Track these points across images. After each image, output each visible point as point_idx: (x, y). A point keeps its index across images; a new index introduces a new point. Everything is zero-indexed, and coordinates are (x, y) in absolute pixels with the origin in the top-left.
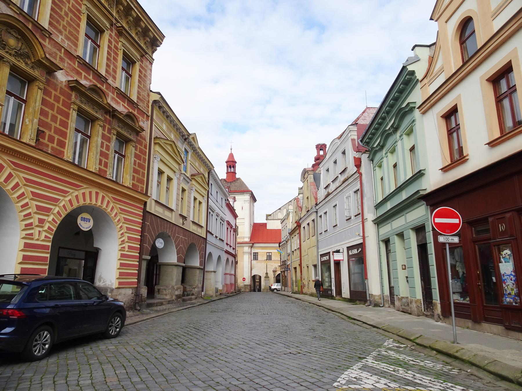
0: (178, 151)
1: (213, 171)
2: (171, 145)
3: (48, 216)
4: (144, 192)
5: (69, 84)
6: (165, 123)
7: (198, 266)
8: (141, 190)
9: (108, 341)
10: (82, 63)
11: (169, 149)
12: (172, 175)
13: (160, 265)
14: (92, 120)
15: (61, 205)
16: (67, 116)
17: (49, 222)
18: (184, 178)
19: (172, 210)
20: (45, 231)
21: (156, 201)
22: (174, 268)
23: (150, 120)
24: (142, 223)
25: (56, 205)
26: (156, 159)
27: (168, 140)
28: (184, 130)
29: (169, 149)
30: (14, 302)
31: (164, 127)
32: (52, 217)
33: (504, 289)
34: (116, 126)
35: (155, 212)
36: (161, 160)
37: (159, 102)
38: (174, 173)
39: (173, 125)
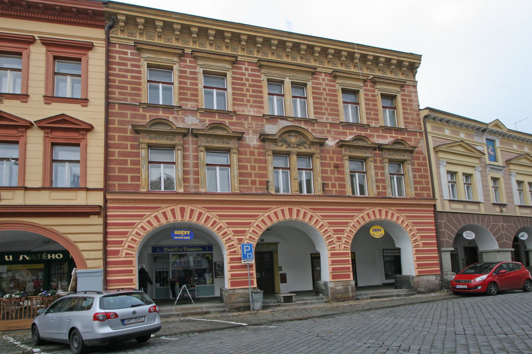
0: (467, 144)
2: (460, 145)
3: (343, 234)
4: (432, 196)
5: (338, 144)
6: (462, 132)
10: (146, 107)
12: (468, 171)
15: (351, 225)
16: (138, 155)
17: (345, 238)
18: (491, 168)
20: (344, 244)
21: (450, 201)
24: (435, 222)
25: (347, 226)
31: (515, 147)
32: (346, 234)
34: (387, 155)
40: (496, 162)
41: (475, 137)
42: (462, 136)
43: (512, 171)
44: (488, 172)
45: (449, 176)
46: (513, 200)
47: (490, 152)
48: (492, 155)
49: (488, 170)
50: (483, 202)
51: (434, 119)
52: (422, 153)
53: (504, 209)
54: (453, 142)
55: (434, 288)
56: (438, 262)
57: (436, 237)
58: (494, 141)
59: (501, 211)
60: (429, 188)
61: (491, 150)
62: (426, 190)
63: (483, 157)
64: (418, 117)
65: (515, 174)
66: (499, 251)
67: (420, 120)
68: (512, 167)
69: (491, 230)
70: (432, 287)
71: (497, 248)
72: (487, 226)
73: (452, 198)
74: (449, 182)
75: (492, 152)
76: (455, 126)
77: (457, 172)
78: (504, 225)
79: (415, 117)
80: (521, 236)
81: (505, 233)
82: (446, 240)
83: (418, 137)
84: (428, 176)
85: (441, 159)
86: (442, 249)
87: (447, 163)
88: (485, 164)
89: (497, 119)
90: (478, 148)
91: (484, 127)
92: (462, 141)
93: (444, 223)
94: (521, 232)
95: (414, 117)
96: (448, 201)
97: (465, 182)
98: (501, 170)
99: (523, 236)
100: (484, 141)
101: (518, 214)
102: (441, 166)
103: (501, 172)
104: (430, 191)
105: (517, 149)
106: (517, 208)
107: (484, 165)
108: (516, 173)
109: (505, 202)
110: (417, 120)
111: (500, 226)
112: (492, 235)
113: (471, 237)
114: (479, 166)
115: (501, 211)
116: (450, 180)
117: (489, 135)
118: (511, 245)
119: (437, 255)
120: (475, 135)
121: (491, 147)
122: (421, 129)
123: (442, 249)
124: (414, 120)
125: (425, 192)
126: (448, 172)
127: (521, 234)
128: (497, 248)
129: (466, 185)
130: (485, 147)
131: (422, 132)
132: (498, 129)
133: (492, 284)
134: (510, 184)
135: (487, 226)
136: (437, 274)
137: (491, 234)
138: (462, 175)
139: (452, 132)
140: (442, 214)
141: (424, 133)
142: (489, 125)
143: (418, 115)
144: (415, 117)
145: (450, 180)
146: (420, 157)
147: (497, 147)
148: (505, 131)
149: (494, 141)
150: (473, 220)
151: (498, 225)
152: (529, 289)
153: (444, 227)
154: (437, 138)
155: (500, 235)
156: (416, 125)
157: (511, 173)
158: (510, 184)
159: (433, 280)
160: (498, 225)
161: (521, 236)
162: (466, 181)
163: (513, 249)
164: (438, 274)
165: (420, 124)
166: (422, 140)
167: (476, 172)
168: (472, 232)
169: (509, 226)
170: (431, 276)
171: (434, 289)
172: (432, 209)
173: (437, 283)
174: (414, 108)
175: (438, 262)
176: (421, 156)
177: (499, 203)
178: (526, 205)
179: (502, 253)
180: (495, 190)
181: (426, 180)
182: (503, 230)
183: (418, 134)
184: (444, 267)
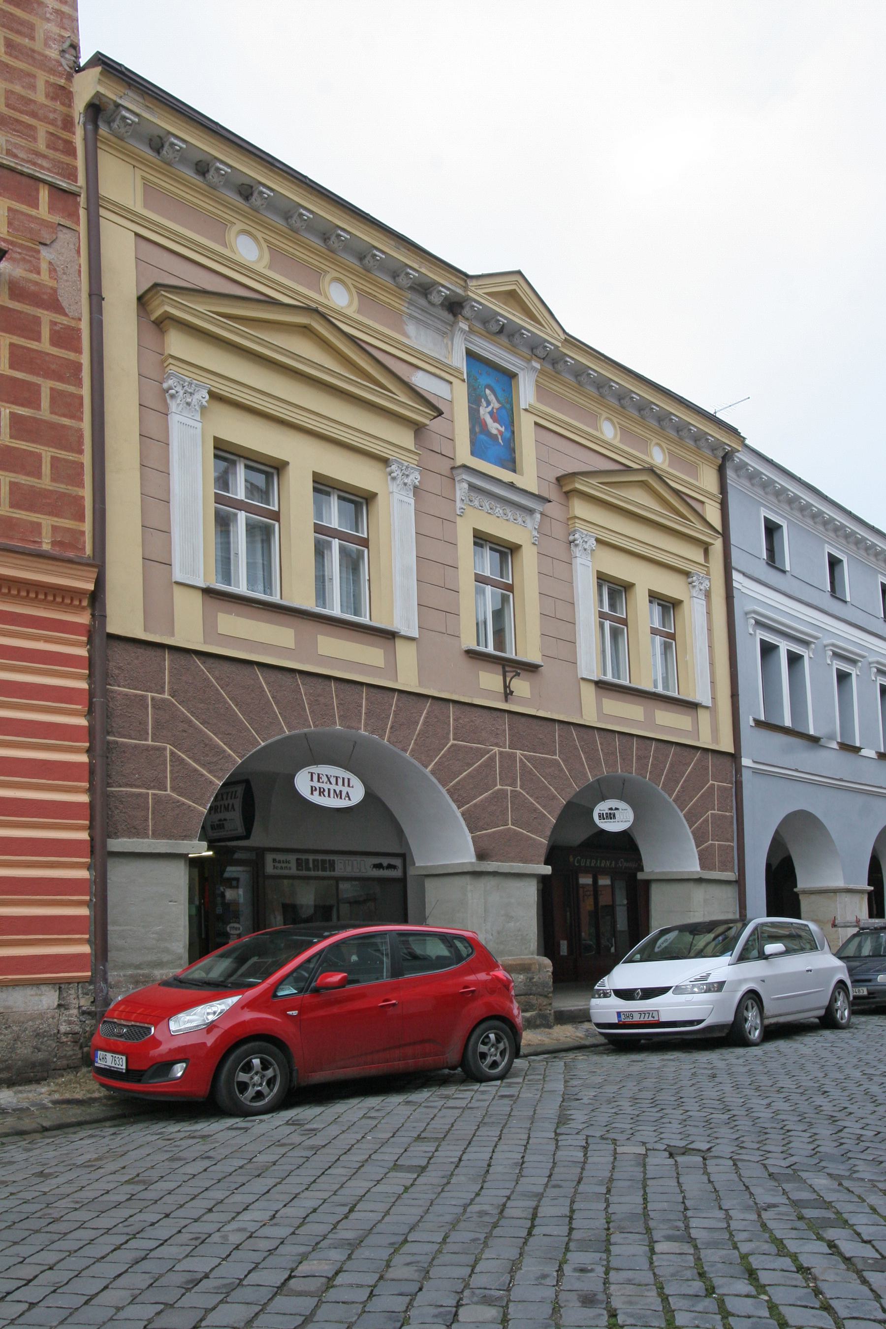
0: (677, 492)
1: (742, 456)
2: (643, 484)
4: (89, 550)
6: (608, 419)
7: (698, 872)
8: (54, 543)
9: (740, 1051)
11: (638, 499)
12: (671, 586)
13: (647, 883)
14: (625, 588)
18: (472, 487)
19: (693, 706)
21: (601, 685)
22: (469, 887)
23: (82, 213)
24: (91, 693)
26: (694, 586)
27: (628, 469)
28: (402, 256)
29: (638, 499)
30: (860, 943)
31: (608, 431)
33: (219, 899)
35: (599, 720)
36: (214, 396)
37: (118, 106)
38: (379, 465)
39: (240, 194)
40: (514, 471)
41: (411, 328)
42: (658, 457)
43: (579, 525)
44: (459, 504)
45: (657, 610)
46: (574, 653)
47: (489, 420)
48: (494, 437)
49: (459, 495)
50: (415, 633)
51: (202, 168)
52: (55, 305)
53: (521, 686)
54: (267, 299)
55: (40, 1056)
56: (84, 911)
57: (86, 774)
58: (512, 376)
59: (508, 694)
60: (78, 501)
61: (491, 414)
62: (54, 512)
63: (436, 425)
64: (58, 105)
65: (593, 542)
66: (700, 881)
67: (68, 124)
68: (580, 508)
69: (443, 774)
70: (24, 1051)
71: (693, 866)
72: (424, 752)
73: (609, 677)
74: (654, 631)
75: (495, 420)
76: (662, 428)
77: (632, 585)
78: (513, 757)
79: (40, 96)
80: (601, 816)
81: (515, 795)
82: (157, 800)
83: (43, 210)
84: (81, 437)
85: (579, 525)
86: (117, 844)
87: (214, 396)
88: (450, 463)
89: (519, 273)
90: (420, 380)
91: (448, 285)
92: (651, 470)
93: (158, 705)
94: (604, 798)
95: (30, 95)
96: (197, 599)
97: (606, 609)
98: (531, 511)
99: (611, 816)
100: (459, 360)
101: (590, 718)
102: (173, 406)
103: (528, 520)
104: (81, 518)
105: (616, 442)
106: (589, 693)
107: (444, 466)
108: (598, 541)
109: (532, 656)
110: (52, 123)
111: (492, 758)
112: (447, 797)
113: (339, 795)
114: (413, 461)
115: (508, 694)
116: (657, 625)
117: (481, 335)
118: (543, 852)
119: (84, 874)
120: (411, 316)
121: (491, 397)
122: (72, 175)
123: (117, 844)
124: (34, 115)
125: (47, 522)
126: (602, 579)
127: (602, 807)
128: (693, 866)
129: (607, 624)
130: (461, 392)
131: (76, 195)
132: (518, 319)
133: (254, 1052)
134: (571, 583)
135: (424, 752)
136: (69, 982)
137: (444, 791)
138: (471, 539)
139: (624, 432)
140: (150, 653)
141: (82, 200)
142: (472, 283)
143: (64, 94)
144: (40, 96)
145: (657, 625)
146: (37, 321)
147: (523, 405)
148: (554, 340)
149: (512, 376)
150: (626, 759)
151: (482, 753)
152: (494, 1064)
153: (157, 724)
154: (166, 255)
155: (488, 800)
156: (41, 146)
157: (574, 533)
158: (570, 583)
159: (41, 1016)
160: (482, 753)
161: (601, 816)
162: (612, 606)
163: (547, 870)
164: (79, 982)
165: (71, 151)
166: (64, 236)
167: (393, 487)
168: (347, 775)
169: (540, 764)
170: (30, 991)
171: (44, 1064)
172: (84, 619)
173: (64, 1028)
174: (38, 46)
175: (84, 911)
176: (46, 316)
177: (675, 695)
178: (375, 624)
179: (492, 882)
180: (665, 643)
181: (63, 454)
182: (508, 777)
183: (44, 194)
184: (113, 940)
